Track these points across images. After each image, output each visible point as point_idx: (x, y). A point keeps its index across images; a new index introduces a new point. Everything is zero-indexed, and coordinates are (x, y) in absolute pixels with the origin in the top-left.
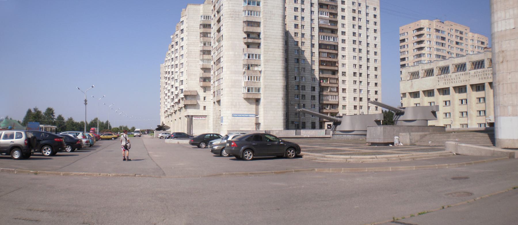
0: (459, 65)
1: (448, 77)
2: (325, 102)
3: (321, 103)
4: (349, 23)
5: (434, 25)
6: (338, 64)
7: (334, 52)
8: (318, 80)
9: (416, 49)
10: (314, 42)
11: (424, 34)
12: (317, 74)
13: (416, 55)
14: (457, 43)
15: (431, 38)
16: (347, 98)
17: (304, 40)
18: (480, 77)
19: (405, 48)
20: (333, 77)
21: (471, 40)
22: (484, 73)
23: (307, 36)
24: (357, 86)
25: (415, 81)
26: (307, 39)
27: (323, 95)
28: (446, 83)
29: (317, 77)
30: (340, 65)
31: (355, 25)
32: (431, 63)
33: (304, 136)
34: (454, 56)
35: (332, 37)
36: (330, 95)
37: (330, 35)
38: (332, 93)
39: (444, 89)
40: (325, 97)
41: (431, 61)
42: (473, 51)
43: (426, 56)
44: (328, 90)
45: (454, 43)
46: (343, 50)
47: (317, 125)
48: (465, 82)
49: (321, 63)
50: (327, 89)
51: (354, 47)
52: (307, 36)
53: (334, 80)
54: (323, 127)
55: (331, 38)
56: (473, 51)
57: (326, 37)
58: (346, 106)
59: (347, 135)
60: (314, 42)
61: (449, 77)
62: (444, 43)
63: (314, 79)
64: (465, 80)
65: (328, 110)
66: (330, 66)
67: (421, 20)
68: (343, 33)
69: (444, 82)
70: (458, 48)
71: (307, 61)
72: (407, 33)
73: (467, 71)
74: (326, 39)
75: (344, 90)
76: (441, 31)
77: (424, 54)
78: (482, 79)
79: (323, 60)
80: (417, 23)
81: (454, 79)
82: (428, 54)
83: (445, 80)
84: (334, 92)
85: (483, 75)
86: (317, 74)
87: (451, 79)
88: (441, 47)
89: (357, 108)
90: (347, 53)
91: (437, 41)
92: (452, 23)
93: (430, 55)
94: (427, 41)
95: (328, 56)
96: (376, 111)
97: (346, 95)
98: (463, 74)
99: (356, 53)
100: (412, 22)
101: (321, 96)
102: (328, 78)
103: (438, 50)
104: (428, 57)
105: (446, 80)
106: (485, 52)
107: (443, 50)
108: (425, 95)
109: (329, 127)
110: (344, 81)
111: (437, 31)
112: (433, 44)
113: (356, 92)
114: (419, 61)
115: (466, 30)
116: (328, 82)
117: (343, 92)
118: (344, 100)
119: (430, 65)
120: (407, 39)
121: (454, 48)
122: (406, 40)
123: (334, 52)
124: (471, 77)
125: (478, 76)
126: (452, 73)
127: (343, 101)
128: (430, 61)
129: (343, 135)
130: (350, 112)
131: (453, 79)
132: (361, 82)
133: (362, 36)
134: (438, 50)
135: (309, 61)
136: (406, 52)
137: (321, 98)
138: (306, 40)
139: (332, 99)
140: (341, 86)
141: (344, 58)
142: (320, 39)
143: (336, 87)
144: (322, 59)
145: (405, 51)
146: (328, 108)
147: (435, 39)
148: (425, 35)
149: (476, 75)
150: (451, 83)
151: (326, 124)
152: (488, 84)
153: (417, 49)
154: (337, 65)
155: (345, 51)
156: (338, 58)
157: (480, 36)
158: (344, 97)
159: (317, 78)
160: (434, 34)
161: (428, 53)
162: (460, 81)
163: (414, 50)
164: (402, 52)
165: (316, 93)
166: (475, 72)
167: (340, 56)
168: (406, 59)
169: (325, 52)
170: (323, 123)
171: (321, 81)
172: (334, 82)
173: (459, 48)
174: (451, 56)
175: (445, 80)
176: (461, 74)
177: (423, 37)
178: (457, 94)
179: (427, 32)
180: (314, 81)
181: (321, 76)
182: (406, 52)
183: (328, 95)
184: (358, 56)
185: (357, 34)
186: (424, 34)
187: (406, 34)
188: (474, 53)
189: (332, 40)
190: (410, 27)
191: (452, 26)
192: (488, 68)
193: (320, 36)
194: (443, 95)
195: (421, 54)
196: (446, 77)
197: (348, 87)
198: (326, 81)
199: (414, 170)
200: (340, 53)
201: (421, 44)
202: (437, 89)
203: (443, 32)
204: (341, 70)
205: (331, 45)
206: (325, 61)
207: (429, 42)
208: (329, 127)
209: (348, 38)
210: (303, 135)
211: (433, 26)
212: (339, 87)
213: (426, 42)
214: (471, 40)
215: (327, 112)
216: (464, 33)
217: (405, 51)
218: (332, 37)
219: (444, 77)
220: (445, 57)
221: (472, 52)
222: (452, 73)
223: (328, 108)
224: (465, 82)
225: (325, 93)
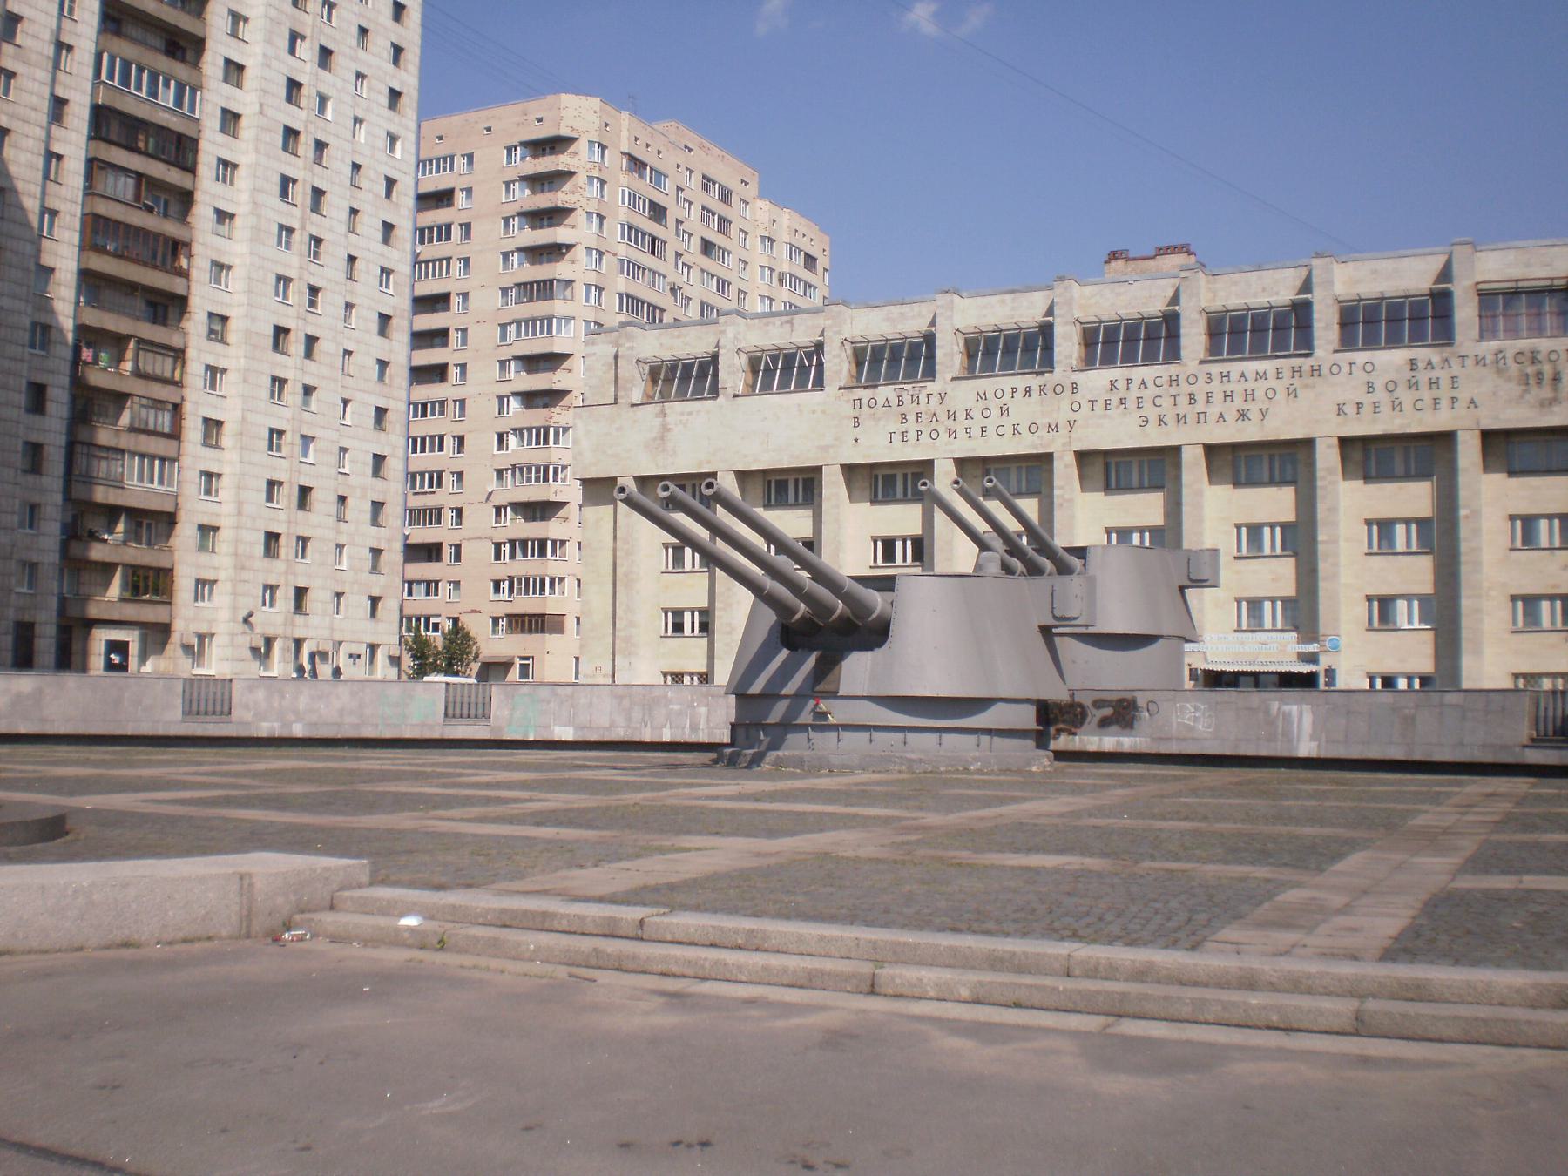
0: (684, 365)
1: (923, 399)
2: (101, 495)
3: (74, 495)
4: (273, 13)
5: (625, 134)
6: (190, 256)
7: (173, 176)
8: (66, 344)
9: (519, 250)
10: (65, 86)
11: (571, 174)
12: (64, 300)
13: (518, 285)
14: (707, 247)
15: (606, 199)
16: (225, 481)
17: (15, 58)
18: (1151, 412)
19: (448, 238)
20: (157, 340)
21: (763, 238)
22: (1173, 391)
23: (36, 37)
24: (285, 415)
25: (690, 413)
26: (34, 57)
27: (91, 445)
28: (912, 435)
29: (68, 324)
30: (200, 269)
31: (303, 38)
32: (797, 319)
33: (265, 729)
34: (693, 312)
35: (173, 83)
36: (133, 454)
37: (163, 63)
38: (143, 437)
39: (881, 473)
40: (104, 464)
41: (600, 325)
42: (771, 300)
43: (576, 298)
44: (118, 416)
45: (696, 245)
46: (224, 181)
47: (46, 642)
48: (1043, 432)
49: (97, 230)
50: (112, 409)
51: (291, 173)
52: (36, 37)
53: (159, 358)
54: (76, 659)
55: (167, 85)
56: (771, 300)
57: (141, 70)
58: (215, 529)
59: (946, 737)
60: (65, 86)
61: (934, 400)
62: (659, 240)
63: (44, 332)
64: (1043, 421)
65: (112, 546)
66: (145, 264)
67: (563, 96)
68: (234, 70)
69: (895, 426)
70: (708, 273)
71: (21, 208)
72: (470, 157)
73: (1059, 374)
74: (139, 88)
75: (213, 426)
76: (652, 169)
77: (569, 283)
78: (1161, 421)
79: (107, 219)
80: (536, 107)
81: (968, 416)
82: (588, 286)
83: (904, 417)
84: (155, 433)
85: (1166, 402)
86: (64, 300)
87: (942, 416)
88: (646, 259)
89: (283, 552)
90: (244, 197)
91: (631, 221)
92: (692, 139)
93: (600, 289)
94: (589, 214)
95: (137, 197)
96: (374, 577)
97: (226, 461)
98: (1028, 391)
99: (297, 212)
100: (505, 100)
101: (78, 448)
102: (129, 337)
103: (635, 269)
104: (587, 300)
105: (912, 418)
106: (1183, 274)
107: (654, 273)
108: (1082, 477)
109: (116, 658)
110: (214, 373)
111: (637, 164)
112: (614, 233)
113: (279, 449)
114: (534, 320)
115: (742, 181)
116: (127, 366)
117: (206, 443)
118: (208, 492)
119: (788, 326)
120: (469, 191)
121: (695, 274)
122: (459, 197)
123: (173, 176)
124: (1086, 407)
125: (1132, 404)
126: (953, 379)
127: (203, 497)
128: (596, 323)
129: (911, 736)
130: (243, 568)
131: (961, 416)
132: (308, 390)
133: (334, 110)
134: (635, 269)
135: (31, 204)
136: (456, 266)
137: (81, 461)
138: (27, 63)
139: (141, 479)
140: (198, 404)
141: (224, 229)
142: (104, 77)
143: (170, 407)
144: (103, 208)
145: (449, 259)
146: (111, 532)
147: (624, 210)
148: (581, 179)
149: (1122, 401)
150: (944, 436)
151: (101, 638)
152: (1200, 451)
153: (523, 254)
154: (185, 267)
155: (232, 184)
156: (189, 219)
157: (801, 224)
158: (209, 476)
159: (61, 330)
160: (622, 179)
161: (592, 279)
162: (1009, 430)
163: (506, 256)
164: (427, 262)
165: (53, 428)
166: (1112, 384)
167: (202, 213)
168: (455, 301)
169: (126, 171)
170: (77, 634)
171: (87, 354)
172: (158, 372)
173: (713, 276)
174: (630, 319)
175: (904, 417)
176: (1014, 390)
177: (567, 187)
178: (1098, 497)
179: (590, 165)
180: (43, 347)
181: (94, 318)
182: (456, 266)
183: (122, 451)
184: (303, 228)
185: (308, 96)
186: (571, 174)
187: (460, 162)
188: (773, 310)
189: (167, 97)
190: (489, 129)
191: (690, 150)
192: (1202, 362)
193: (105, 56)
194: (874, 500)
195: (551, 281)
196: (907, 399)
197: (238, 414)
198: (111, 359)
199: (397, 939)
200: (209, 192)
201: (550, 226)
202: (843, 466)
203: (658, 177)
204: (203, 298)
205: (162, 128)
206: (117, 223)
207: (595, 219)
208: (116, 658)
209: (261, 105)
210: (248, 716)
211: (619, 136)
212: (188, 408)
213: (579, 217)
214: (763, 238)
215: (107, 559)
216: (735, 199)
217: (449, 259)
218: (173, 83)
219: (894, 401)
220: (662, 310)
221: (767, 302)
222: (953, 379)
223: (111, 532)
224: (1043, 432)
225: (104, 436)
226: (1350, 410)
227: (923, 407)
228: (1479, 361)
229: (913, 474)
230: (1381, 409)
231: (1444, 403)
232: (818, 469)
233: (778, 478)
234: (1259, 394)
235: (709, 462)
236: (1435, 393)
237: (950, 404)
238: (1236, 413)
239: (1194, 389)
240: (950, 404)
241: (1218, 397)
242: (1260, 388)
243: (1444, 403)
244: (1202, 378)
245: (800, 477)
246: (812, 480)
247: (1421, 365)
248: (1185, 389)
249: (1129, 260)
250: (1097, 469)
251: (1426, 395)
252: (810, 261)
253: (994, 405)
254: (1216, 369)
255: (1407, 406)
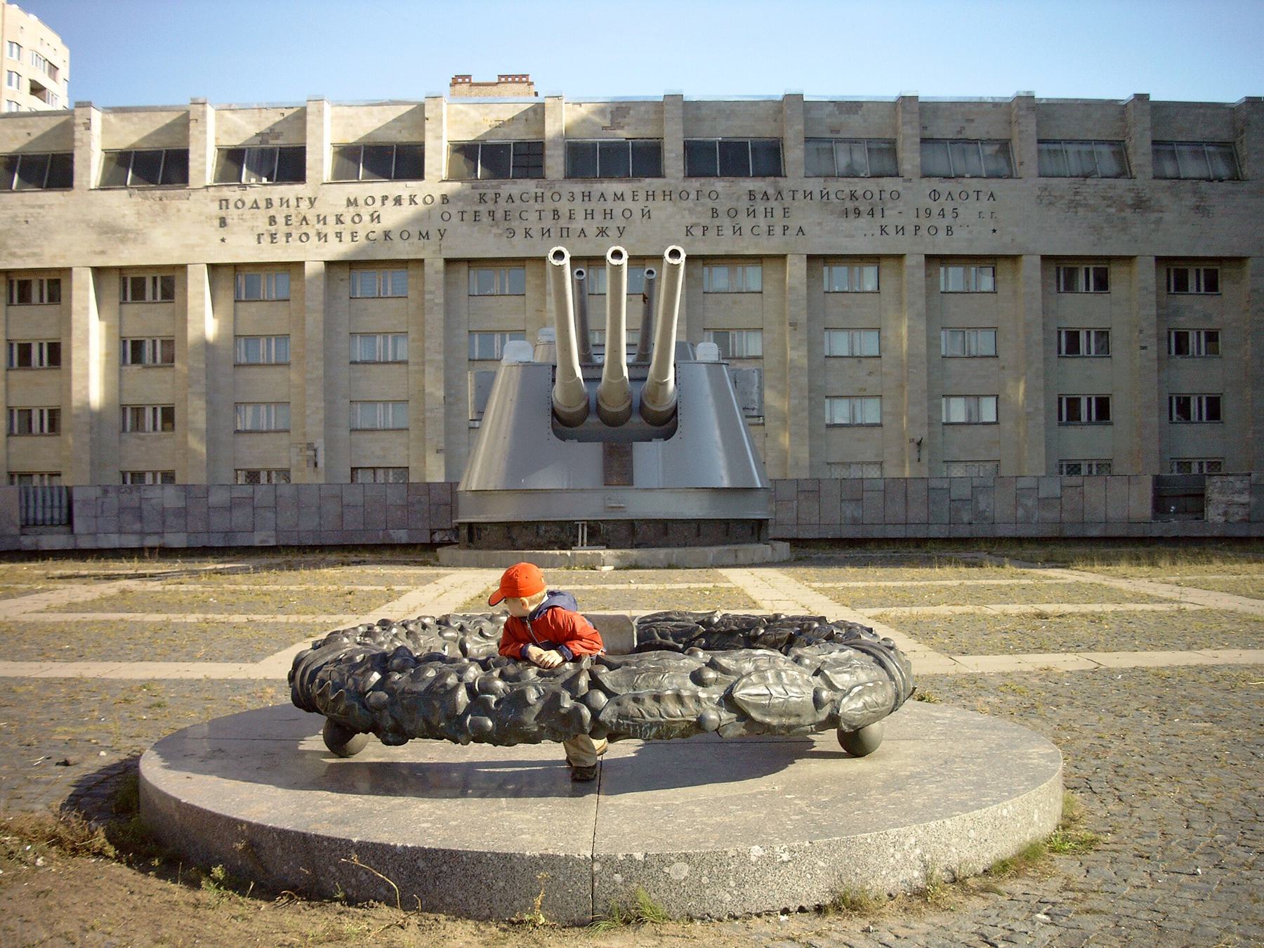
81: (339, 220)
131: (331, 220)
150: (314, 238)
226: (697, 232)
227: (292, 211)
228: (808, 195)
229: (49, 280)
230: (724, 232)
231: (778, 230)
232: (183, 268)
233: (21, 278)
234: (617, 212)
235: (64, 257)
236: (770, 220)
237: (320, 208)
238: (595, 229)
239: (557, 205)
240: (320, 208)
241: (580, 215)
242: (618, 207)
243: (778, 230)
244: (566, 196)
245: (45, 279)
246: (58, 282)
247: (759, 196)
248: (549, 205)
249: (472, 85)
250: (114, 285)
251: (762, 221)
252: (53, 69)
253: (366, 213)
254: (578, 188)
255: (746, 230)
